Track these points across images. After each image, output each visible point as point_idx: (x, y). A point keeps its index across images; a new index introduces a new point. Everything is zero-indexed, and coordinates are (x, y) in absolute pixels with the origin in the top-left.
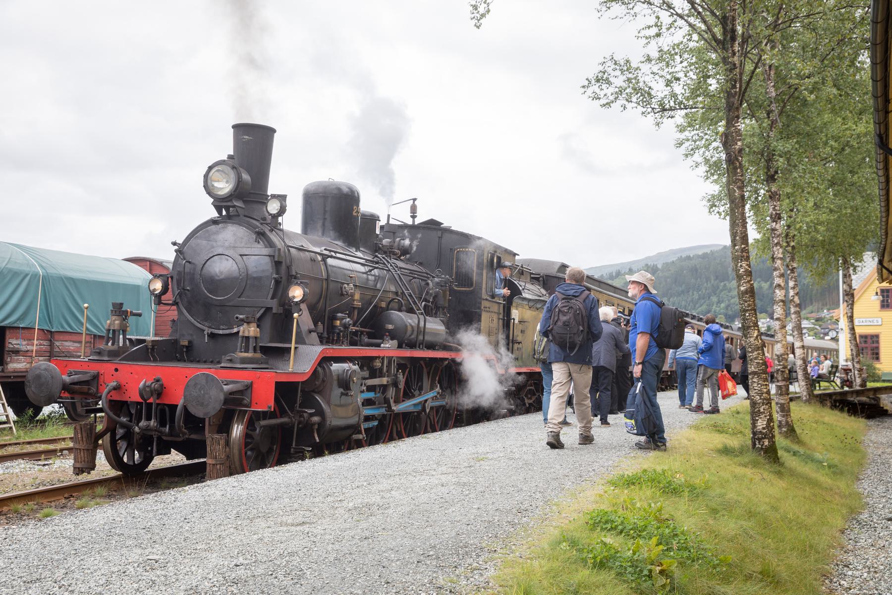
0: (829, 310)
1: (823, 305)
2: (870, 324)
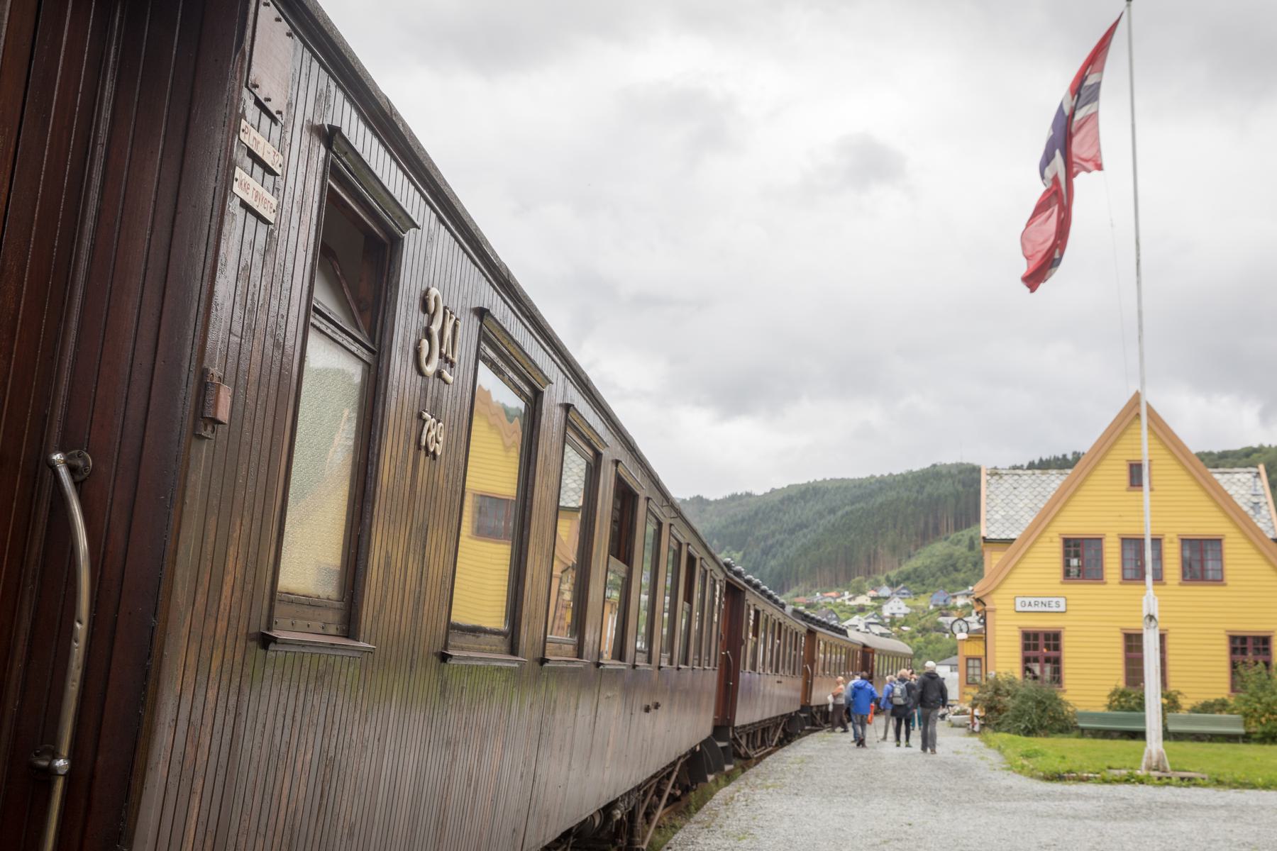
2: (1044, 609)
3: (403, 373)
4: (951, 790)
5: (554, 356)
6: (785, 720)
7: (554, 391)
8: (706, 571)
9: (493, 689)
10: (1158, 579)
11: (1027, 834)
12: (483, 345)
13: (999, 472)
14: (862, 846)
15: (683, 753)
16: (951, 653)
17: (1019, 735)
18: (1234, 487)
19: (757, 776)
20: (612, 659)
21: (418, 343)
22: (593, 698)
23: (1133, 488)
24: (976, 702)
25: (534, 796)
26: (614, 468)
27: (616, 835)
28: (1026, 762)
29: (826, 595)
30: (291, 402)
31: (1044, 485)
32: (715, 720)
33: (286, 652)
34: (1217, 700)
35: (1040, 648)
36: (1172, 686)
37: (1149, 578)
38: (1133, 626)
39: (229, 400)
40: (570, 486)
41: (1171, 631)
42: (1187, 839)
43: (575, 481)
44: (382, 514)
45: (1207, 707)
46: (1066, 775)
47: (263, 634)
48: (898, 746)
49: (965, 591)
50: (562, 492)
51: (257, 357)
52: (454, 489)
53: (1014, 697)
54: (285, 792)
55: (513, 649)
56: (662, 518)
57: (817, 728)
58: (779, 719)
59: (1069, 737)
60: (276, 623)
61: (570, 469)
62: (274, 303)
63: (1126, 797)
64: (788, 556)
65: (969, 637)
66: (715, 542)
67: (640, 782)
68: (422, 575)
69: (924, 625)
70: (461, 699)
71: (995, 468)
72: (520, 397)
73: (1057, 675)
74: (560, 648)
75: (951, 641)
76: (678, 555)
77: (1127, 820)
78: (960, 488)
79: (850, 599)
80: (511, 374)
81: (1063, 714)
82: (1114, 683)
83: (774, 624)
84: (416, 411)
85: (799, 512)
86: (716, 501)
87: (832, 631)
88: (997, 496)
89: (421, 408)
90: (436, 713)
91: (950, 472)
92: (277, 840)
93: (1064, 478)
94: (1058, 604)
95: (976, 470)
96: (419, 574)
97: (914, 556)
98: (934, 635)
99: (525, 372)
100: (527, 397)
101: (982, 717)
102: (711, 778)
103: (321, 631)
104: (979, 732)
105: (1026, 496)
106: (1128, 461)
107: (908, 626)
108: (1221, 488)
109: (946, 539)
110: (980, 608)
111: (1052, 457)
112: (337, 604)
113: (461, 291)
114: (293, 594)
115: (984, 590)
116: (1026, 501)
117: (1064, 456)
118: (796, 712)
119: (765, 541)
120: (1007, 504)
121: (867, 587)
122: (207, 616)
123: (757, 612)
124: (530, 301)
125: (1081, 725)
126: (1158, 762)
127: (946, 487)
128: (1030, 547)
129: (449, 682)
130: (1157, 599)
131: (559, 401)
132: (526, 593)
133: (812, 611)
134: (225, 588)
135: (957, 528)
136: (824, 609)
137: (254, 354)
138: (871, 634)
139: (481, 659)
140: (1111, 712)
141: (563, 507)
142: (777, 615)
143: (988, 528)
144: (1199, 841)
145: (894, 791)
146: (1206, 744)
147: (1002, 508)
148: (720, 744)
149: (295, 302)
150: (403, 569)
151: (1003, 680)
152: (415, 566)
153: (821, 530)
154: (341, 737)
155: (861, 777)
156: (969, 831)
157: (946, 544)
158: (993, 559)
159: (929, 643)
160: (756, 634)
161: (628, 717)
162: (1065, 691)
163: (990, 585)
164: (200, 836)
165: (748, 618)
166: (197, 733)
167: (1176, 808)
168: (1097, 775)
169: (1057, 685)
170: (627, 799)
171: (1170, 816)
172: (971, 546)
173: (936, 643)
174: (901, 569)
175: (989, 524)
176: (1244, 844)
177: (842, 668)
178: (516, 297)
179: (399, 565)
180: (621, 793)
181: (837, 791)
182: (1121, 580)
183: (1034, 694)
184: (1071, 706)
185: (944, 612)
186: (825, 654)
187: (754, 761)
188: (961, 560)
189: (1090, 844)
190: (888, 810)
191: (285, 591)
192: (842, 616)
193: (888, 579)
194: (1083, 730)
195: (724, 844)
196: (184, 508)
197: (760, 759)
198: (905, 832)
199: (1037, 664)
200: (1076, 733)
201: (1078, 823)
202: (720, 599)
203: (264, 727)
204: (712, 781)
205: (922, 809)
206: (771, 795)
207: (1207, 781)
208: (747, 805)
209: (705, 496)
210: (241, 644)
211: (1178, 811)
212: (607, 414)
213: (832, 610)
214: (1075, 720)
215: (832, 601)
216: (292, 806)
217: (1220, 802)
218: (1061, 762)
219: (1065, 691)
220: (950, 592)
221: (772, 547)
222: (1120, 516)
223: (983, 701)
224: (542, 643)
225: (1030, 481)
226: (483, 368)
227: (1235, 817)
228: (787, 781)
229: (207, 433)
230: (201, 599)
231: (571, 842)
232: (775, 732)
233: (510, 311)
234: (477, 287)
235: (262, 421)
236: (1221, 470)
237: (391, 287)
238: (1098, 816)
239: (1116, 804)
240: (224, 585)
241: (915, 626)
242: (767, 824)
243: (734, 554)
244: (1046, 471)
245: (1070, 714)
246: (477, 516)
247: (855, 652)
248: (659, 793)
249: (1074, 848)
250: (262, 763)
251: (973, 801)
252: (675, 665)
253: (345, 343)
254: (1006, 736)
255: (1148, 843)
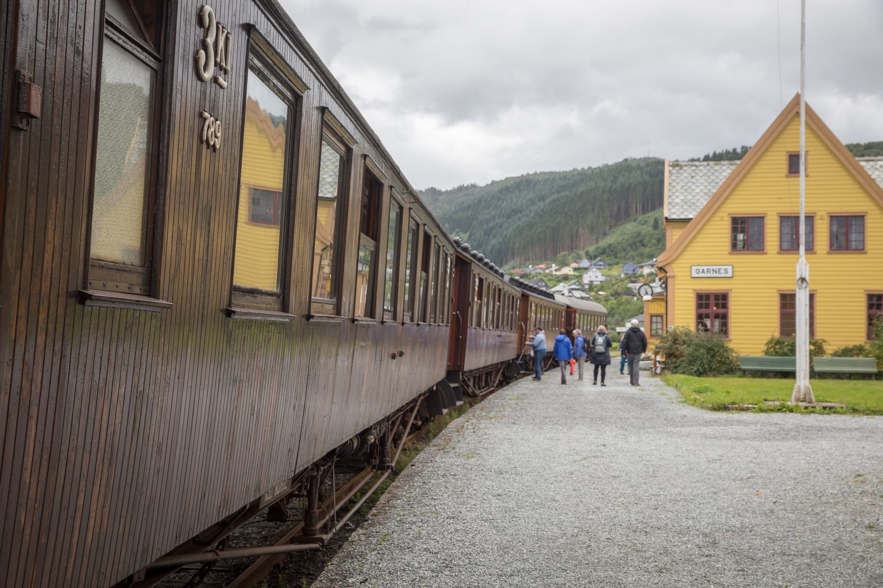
0: (533, 265)
1: (526, 260)
3: (185, 79)
4: (637, 418)
5: (311, 66)
6: (504, 366)
7: (312, 96)
8: (439, 247)
9: (270, 338)
10: (810, 249)
11: (697, 452)
12: (251, 56)
13: (680, 164)
14: (566, 462)
15: (423, 391)
16: (638, 312)
17: (693, 376)
18: (877, 173)
19: (482, 410)
20: (365, 316)
21: (196, 53)
22: (350, 347)
23: (791, 175)
24: (658, 350)
25: (305, 424)
26: (363, 161)
27: (370, 456)
28: (698, 397)
29: (537, 267)
30: (93, 100)
31: (717, 174)
32: (448, 366)
33: (100, 307)
34: (855, 346)
35: (711, 307)
36: (818, 336)
37: (802, 248)
38: (787, 288)
39: (40, 98)
40: (327, 180)
41: (819, 291)
42: (827, 454)
43: (330, 176)
44: (173, 195)
45: (846, 352)
46: (730, 406)
47: (80, 292)
48: (595, 384)
49: (650, 262)
50: (320, 185)
51: (60, 61)
52: (232, 176)
53: (689, 346)
54: (105, 418)
55: (285, 307)
56: (402, 203)
57: (530, 372)
58: (499, 365)
59: (733, 377)
60: (90, 284)
61: (327, 166)
62: (72, 15)
63: (779, 422)
64: (506, 236)
65: (653, 299)
66: (446, 225)
67: (389, 414)
68: (208, 247)
69: (617, 290)
70: (244, 346)
71: (677, 161)
72: (283, 101)
73: (724, 328)
74: (323, 307)
75: (638, 302)
76: (416, 233)
77: (778, 440)
78: (647, 178)
79: (556, 270)
80: (275, 81)
81: (728, 358)
82: (771, 333)
83: (495, 290)
84: (197, 110)
85: (515, 200)
86: (447, 192)
87: (542, 295)
88: (678, 183)
89: (201, 109)
90: (224, 357)
91: (639, 165)
92: (100, 455)
93: (733, 167)
94: (726, 271)
95: (660, 163)
96: (206, 246)
97: (609, 234)
98: (624, 298)
99: (287, 79)
100: (289, 100)
101: (663, 362)
102: (445, 411)
103: (128, 291)
104: (660, 374)
105: (702, 183)
106: (787, 152)
107: (604, 291)
108: (866, 173)
109: (635, 220)
110: (663, 275)
111: (724, 151)
112: (140, 270)
113: (231, 7)
114: (103, 261)
115: (665, 260)
116: (702, 187)
117: (735, 150)
118: (513, 360)
119: (487, 225)
120: (686, 190)
121: (570, 260)
122: (33, 277)
123: (481, 280)
124: (289, 19)
125: (743, 367)
126: (805, 395)
127: (635, 177)
128: (705, 224)
129: (233, 333)
130: (808, 265)
131: (316, 104)
132: (293, 263)
133: (526, 280)
134: (46, 255)
135: (644, 211)
136: (535, 278)
137: (58, 59)
138: (573, 298)
139: (258, 315)
140: (767, 357)
141: (322, 197)
142: (497, 282)
143: (669, 210)
144: (837, 455)
145: (592, 420)
146: (845, 381)
147: (682, 193)
148: (452, 385)
149: (90, 15)
150: (192, 241)
151: (681, 333)
152: (202, 239)
153: (533, 214)
154: (148, 375)
155: (566, 410)
156: (651, 450)
157: (635, 224)
158: (674, 235)
159: (620, 304)
160: (480, 298)
161: (378, 363)
162: (730, 341)
163: (671, 256)
164: (38, 451)
165: (474, 285)
166: (31, 371)
167: (819, 430)
168: (755, 406)
169: (724, 336)
170: (378, 427)
171: (814, 437)
172: (656, 226)
173: (627, 305)
174: (598, 245)
175: (670, 207)
176: (873, 458)
177: (550, 325)
178: (277, 15)
179: (189, 238)
180: (374, 422)
181: (547, 421)
182: (779, 251)
183: (705, 343)
184: (736, 353)
185: (633, 279)
186: (536, 314)
187: (480, 398)
188: (647, 238)
189: (749, 459)
190: (586, 434)
191: (96, 258)
192: (550, 284)
193: (587, 253)
194: (744, 371)
195: (456, 461)
196: (8, 188)
197: (484, 397)
198: (601, 451)
199: (709, 320)
200: (739, 373)
201: (739, 443)
202: (451, 269)
203: (85, 366)
204: (446, 414)
205: (614, 433)
206: (494, 424)
207: (845, 409)
208: (474, 432)
209: (438, 187)
210: (62, 300)
211: (820, 433)
212: (356, 115)
213: (542, 279)
214: (738, 363)
215: (542, 272)
216: (111, 429)
217: (854, 425)
218: (726, 396)
219: (730, 341)
220: (639, 263)
221: (492, 229)
222: (780, 198)
223: (664, 349)
224: (307, 303)
225: (705, 171)
226: (252, 76)
227: (867, 437)
228: (506, 413)
229: (24, 125)
230: (27, 263)
231: (335, 460)
232: (496, 375)
233: (272, 27)
234: (244, 6)
235: (69, 117)
236: (866, 158)
237: (171, 4)
238: (755, 438)
239: (770, 428)
240: (45, 252)
241: (609, 291)
242: (490, 446)
243: (462, 235)
244: (718, 162)
245: (735, 359)
246: (251, 206)
247: (560, 312)
248: (404, 423)
249: (736, 461)
250: (85, 395)
251: (655, 427)
252: (415, 322)
253: (134, 52)
254: (682, 377)
255: (795, 458)
